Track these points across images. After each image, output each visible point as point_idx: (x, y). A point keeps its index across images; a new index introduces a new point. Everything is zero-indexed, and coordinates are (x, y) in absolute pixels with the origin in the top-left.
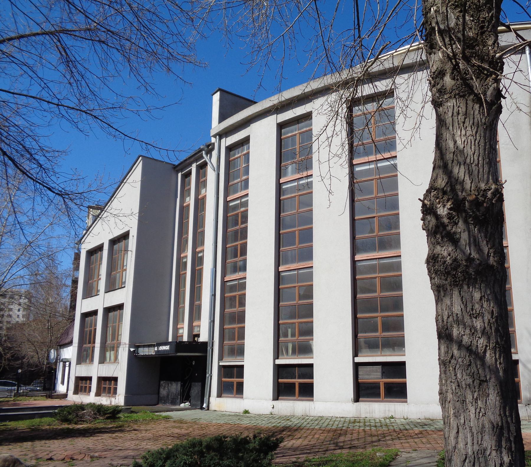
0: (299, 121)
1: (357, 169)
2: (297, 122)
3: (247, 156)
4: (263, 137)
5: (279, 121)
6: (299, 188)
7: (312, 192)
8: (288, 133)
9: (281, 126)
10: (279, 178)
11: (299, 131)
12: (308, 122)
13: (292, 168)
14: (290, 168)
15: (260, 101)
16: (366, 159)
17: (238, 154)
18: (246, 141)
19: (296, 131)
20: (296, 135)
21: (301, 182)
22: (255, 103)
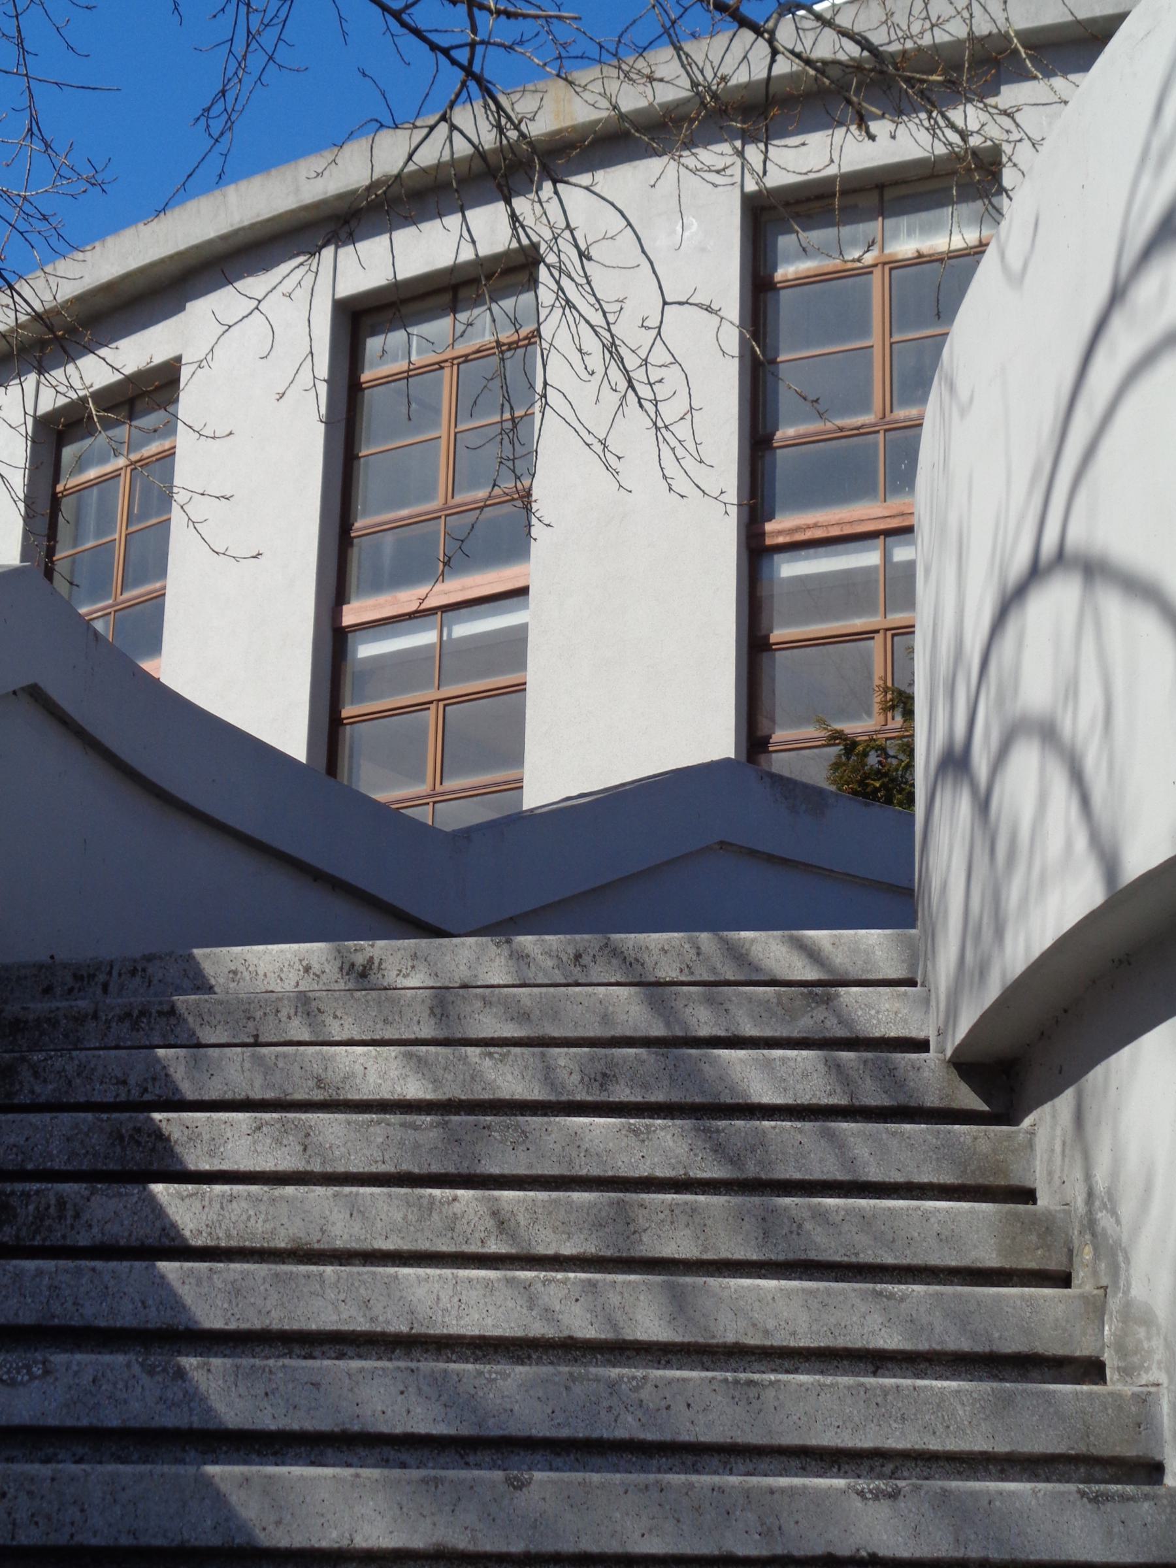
1: (366, 650)
6: (446, 658)
7: (520, 688)
9: (358, 319)
16: (406, 599)
18: (156, 389)
20: (115, 476)
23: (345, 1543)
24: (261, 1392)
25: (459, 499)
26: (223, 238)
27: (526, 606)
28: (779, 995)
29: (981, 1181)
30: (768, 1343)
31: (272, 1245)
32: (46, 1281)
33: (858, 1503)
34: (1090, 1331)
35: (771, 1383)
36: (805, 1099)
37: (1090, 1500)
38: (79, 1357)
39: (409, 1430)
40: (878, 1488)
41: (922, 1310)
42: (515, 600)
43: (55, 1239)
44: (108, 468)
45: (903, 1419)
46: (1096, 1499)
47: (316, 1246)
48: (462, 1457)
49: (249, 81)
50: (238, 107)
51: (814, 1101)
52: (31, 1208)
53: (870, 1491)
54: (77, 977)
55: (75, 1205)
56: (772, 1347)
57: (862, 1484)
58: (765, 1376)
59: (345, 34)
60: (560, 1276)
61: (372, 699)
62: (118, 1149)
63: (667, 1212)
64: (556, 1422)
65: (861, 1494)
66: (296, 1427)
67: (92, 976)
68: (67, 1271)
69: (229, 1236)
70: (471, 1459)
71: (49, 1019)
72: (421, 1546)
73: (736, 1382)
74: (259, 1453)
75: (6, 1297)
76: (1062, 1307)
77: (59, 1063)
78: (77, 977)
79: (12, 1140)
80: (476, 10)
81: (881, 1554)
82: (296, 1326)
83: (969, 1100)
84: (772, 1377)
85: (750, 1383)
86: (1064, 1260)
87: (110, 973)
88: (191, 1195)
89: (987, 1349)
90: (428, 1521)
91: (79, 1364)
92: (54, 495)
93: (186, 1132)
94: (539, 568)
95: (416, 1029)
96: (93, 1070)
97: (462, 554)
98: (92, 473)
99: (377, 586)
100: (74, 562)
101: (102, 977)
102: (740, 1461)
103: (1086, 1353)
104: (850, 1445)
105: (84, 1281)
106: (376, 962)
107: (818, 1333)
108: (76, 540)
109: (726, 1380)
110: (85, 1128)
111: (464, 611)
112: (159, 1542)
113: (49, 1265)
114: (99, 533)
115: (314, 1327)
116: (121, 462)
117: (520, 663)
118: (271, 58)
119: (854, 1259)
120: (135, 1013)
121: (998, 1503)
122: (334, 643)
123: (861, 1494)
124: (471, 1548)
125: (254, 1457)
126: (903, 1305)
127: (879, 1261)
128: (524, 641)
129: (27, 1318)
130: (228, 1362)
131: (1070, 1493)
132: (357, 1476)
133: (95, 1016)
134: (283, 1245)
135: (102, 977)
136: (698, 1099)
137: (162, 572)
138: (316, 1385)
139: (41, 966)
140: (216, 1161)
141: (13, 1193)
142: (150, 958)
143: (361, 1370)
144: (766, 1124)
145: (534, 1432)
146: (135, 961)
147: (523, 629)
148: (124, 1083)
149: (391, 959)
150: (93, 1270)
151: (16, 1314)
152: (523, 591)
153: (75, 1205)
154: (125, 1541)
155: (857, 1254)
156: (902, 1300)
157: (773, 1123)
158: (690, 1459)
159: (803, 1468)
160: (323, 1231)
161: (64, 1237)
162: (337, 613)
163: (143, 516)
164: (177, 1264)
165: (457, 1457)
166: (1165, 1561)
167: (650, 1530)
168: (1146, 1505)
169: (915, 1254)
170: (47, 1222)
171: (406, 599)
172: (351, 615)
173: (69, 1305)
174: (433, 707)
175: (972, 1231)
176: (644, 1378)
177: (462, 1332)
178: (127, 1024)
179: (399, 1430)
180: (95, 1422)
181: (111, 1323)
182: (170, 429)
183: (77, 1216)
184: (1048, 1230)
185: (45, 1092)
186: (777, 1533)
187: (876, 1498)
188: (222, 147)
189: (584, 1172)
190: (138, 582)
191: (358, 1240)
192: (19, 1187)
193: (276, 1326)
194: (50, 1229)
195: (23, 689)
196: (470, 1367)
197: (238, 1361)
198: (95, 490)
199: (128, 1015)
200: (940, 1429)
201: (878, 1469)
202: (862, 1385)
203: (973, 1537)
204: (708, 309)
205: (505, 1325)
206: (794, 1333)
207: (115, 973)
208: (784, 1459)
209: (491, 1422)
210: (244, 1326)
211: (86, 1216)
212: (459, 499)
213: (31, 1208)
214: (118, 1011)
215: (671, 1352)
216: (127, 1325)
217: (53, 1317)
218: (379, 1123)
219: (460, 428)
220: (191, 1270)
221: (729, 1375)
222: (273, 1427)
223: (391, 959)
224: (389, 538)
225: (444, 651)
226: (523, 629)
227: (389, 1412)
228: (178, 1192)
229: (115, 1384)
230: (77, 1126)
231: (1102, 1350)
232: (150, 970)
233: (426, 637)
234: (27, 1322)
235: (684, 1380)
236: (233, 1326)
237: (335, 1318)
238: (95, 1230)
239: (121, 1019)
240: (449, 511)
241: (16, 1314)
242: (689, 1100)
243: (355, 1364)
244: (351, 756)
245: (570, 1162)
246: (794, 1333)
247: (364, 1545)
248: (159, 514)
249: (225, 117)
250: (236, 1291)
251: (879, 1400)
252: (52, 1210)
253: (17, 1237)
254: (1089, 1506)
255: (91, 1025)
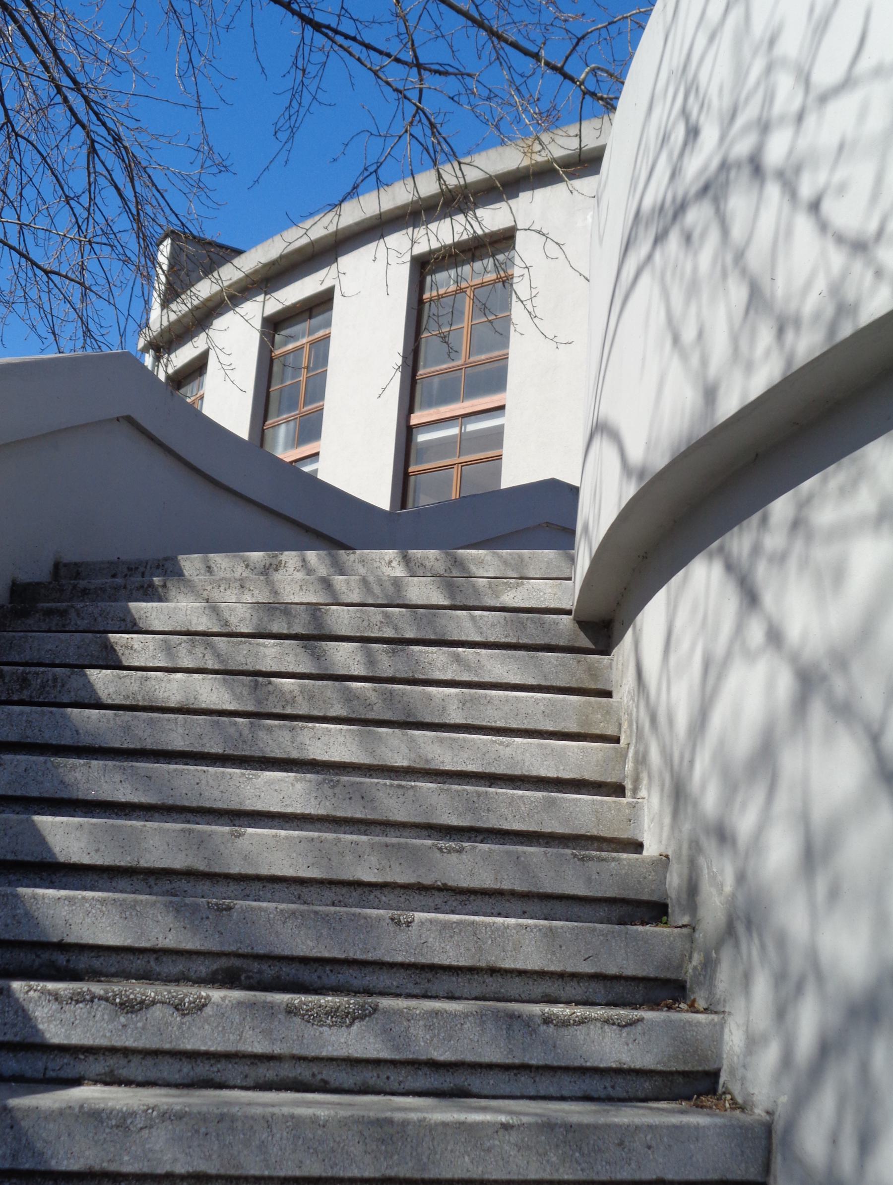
0: (314, 312)
1: (422, 438)
2: (307, 314)
3: (321, 347)
4: (370, 293)
5: (421, 248)
6: (464, 442)
7: (499, 458)
8: (443, 282)
9: (422, 267)
10: (406, 411)
11: (311, 338)
12: (326, 315)
13: (287, 431)
14: (282, 431)
15: (250, 248)
16: (446, 411)
17: (295, 341)
18: (322, 303)
19: (303, 336)
20: (301, 348)
21: (472, 427)
22: (239, 252)
23: (134, 863)
24: (118, 780)
25: (472, 359)
26: (357, 224)
27: (504, 416)
28: (490, 583)
29: (580, 685)
30: (427, 767)
31: (167, 705)
32: (24, 718)
33: (438, 855)
34: (617, 768)
35: (412, 787)
36: (492, 639)
37: (579, 859)
38: (18, 757)
39: (200, 805)
40: (450, 846)
41: (518, 752)
42: (499, 412)
43: (51, 698)
44: (298, 344)
45: (488, 810)
46: (582, 859)
47: (191, 706)
48: (232, 821)
49: (302, 111)
50: (297, 125)
51: (497, 640)
52: (39, 681)
53: (446, 848)
54: (129, 569)
55: (62, 680)
56: (430, 769)
57: (442, 844)
58: (409, 783)
59: (353, 84)
60: (310, 725)
61: (426, 462)
62: (104, 654)
63: (388, 694)
64: (285, 803)
65: (440, 849)
66: (136, 800)
67: (137, 568)
68: (36, 713)
69: (144, 700)
70: (237, 822)
71: (101, 588)
72: (178, 867)
73: (391, 785)
74: (117, 814)
75: (3, 726)
76: (602, 753)
77: (90, 609)
78: (129, 569)
79: (49, 647)
80: (422, 71)
81: (450, 884)
82: (160, 747)
83: (584, 641)
84: (413, 784)
85: (399, 786)
86: (616, 729)
87: (146, 567)
88: (125, 677)
89: (555, 776)
90: (184, 853)
91: (18, 761)
92: (271, 357)
93: (141, 645)
94: (509, 397)
95: (292, 597)
96: (108, 613)
97: (474, 391)
98: (290, 347)
99: (431, 403)
100: (281, 393)
101: (142, 569)
102: (392, 830)
103: (614, 780)
104: (456, 824)
105: (45, 718)
106: (283, 562)
107: (457, 762)
108: (282, 381)
109: (385, 784)
110: (87, 641)
111: (473, 417)
112: (29, 858)
113: (27, 709)
114: (293, 377)
115: (170, 748)
116: (305, 340)
117: (499, 444)
118: (314, 98)
119: (493, 724)
120: (146, 586)
121: (522, 859)
122: (406, 434)
123: (440, 849)
124: (207, 870)
125: (114, 816)
126: (508, 749)
127: (508, 726)
128: (503, 433)
129: (13, 737)
130: (101, 762)
131: (567, 855)
132: (145, 826)
133: (125, 587)
134: (173, 705)
135: (142, 569)
136: (433, 637)
137: (322, 397)
138: (149, 777)
139: (111, 563)
140: (156, 661)
141: (29, 672)
142: (166, 559)
143: (175, 770)
144: (460, 650)
145: (272, 809)
146: (159, 560)
147: (501, 428)
148: (124, 620)
149: (291, 561)
150: (51, 712)
151: (7, 736)
152: (502, 408)
153: (62, 680)
154: (10, 857)
155: (495, 722)
156: (507, 746)
157: (464, 649)
158: (363, 828)
159: (429, 836)
160: (195, 698)
161: (55, 697)
162: (408, 419)
163: (315, 368)
164: (97, 711)
165: (229, 821)
166: (622, 896)
167: (313, 864)
168: (613, 864)
169: (529, 723)
170: (47, 689)
171: (446, 411)
172: (415, 419)
173: (36, 731)
174: (455, 466)
175: (570, 711)
176: (338, 781)
177: (253, 754)
178: (141, 592)
179: (195, 804)
180: (24, 793)
181: (59, 742)
182: (328, 324)
183: (63, 686)
184: (608, 712)
185: (83, 624)
186: (388, 869)
187: (449, 852)
188: (288, 146)
189: (356, 673)
190: (311, 403)
191: (215, 704)
192: (33, 669)
193: (149, 747)
194: (48, 693)
195: (123, 417)
196: (238, 771)
197: (107, 762)
198: (292, 355)
199: (142, 587)
200: (510, 817)
201: (473, 839)
202: (465, 790)
203: (506, 877)
204: (539, 232)
205: (277, 751)
206: (443, 762)
207: (148, 567)
208: (419, 830)
209: (248, 802)
210: (132, 746)
211: (67, 686)
212: (472, 359)
213: (39, 681)
214: (137, 585)
215: (373, 770)
216: (67, 743)
217: (27, 737)
218: (245, 643)
219: (474, 322)
220: (104, 714)
221: (388, 782)
222: (123, 800)
223: (291, 561)
224: (436, 380)
225: (463, 438)
226: (501, 428)
227: (189, 794)
228: (118, 675)
229: (37, 773)
230: (83, 640)
231: (625, 777)
232: (166, 566)
233: (454, 431)
234: (13, 740)
235: (361, 783)
236: (125, 746)
237: (182, 743)
238: (72, 694)
239: (138, 589)
240: (467, 366)
241: (7, 736)
242: (427, 637)
243: (172, 767)
244: (415, 492)
245: (349, 667)
246: (443, 762)
247: (146, 865)
248: (322, 367)
249: (290, 130)
250: (127, 729)
251: (475, 799)
252: (50, 682)
253: (31, 697)
254: (578, 863)
255: (123, 591)
